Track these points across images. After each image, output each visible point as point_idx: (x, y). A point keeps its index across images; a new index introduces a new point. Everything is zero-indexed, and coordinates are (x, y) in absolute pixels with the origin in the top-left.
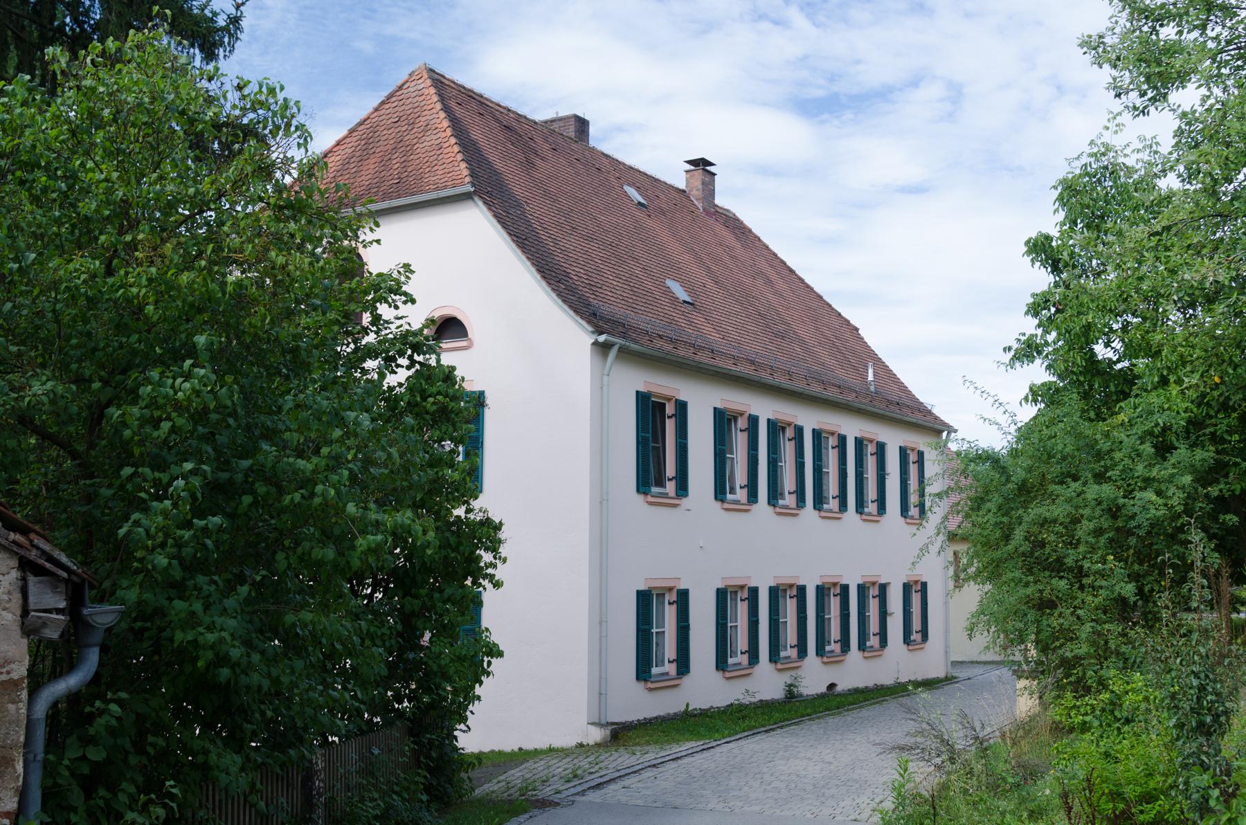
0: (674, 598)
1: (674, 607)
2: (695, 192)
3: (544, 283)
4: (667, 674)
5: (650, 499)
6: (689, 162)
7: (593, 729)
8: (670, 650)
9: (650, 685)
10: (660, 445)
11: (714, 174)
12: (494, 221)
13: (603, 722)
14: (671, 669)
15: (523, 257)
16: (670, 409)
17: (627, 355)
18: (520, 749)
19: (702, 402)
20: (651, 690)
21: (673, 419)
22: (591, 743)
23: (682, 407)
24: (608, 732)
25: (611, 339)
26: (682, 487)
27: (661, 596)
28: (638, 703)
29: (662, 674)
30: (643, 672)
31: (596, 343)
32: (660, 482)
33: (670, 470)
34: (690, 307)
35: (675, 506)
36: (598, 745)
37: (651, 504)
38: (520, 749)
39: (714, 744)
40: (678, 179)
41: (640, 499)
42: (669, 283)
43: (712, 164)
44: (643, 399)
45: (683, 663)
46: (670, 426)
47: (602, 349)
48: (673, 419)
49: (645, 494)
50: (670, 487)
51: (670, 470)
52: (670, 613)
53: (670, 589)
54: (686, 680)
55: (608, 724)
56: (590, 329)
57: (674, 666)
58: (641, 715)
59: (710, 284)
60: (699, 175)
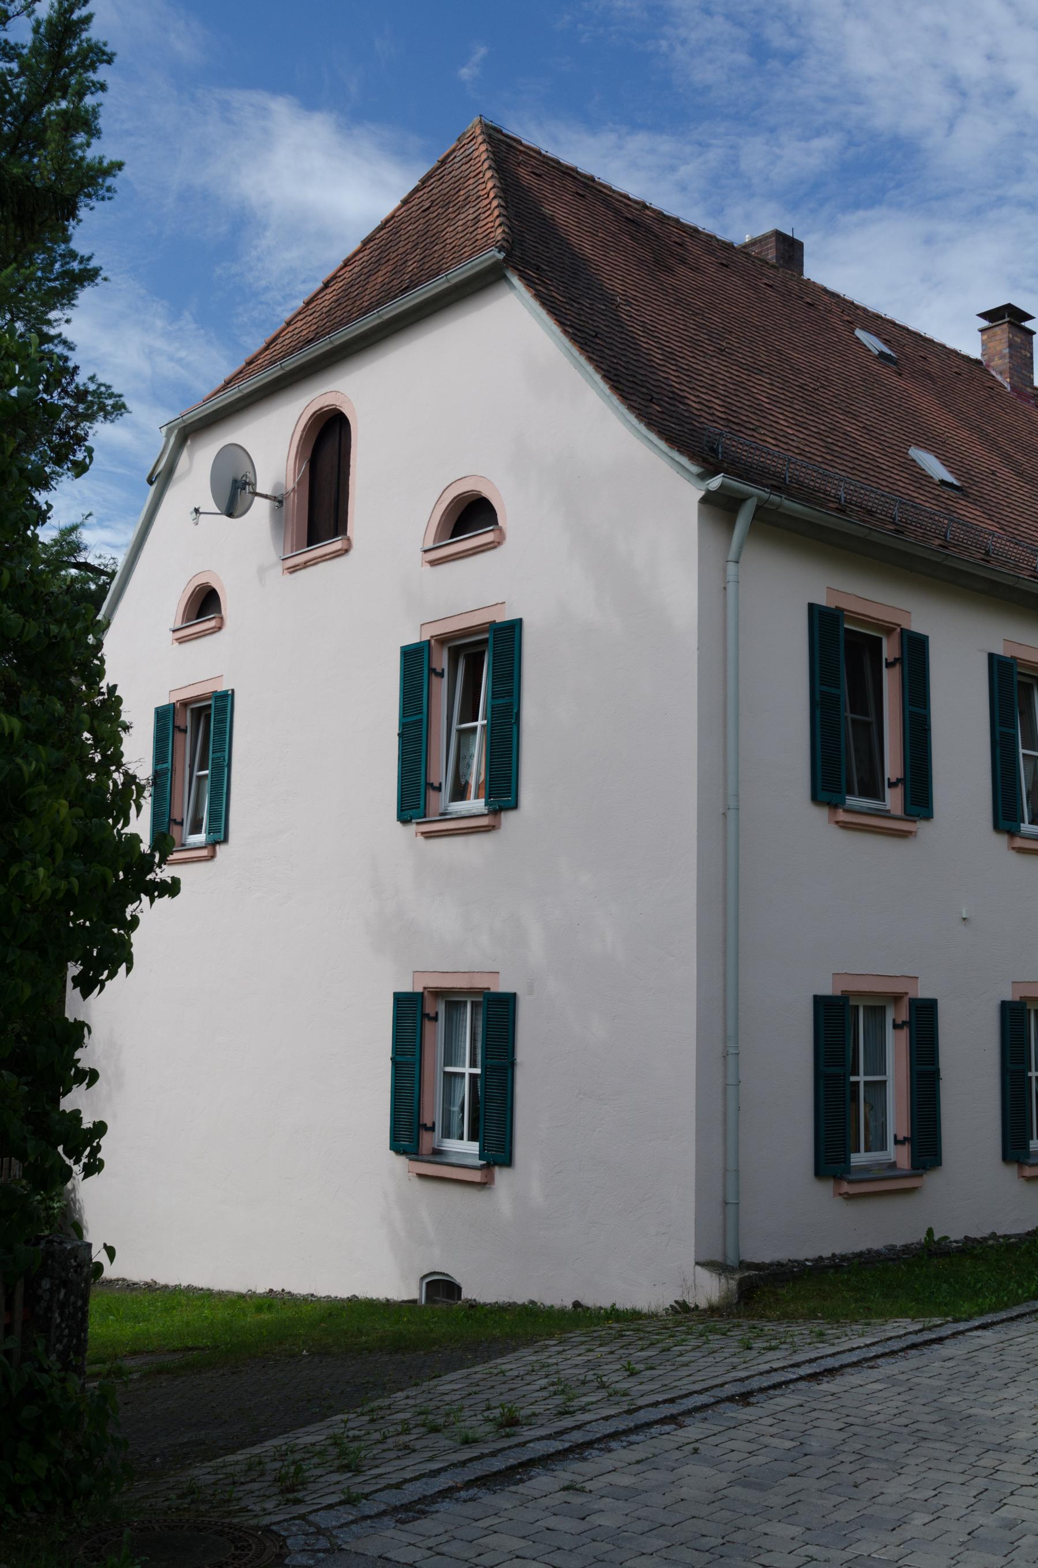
0: (904, 1015)
1: (904, 1033)
2: (997, 362)
3: (615, 400)
4: (893, 1165)
5: (842, 816)
6: (984, 315)
7: (703, 1274)
8: (897, 1118)
9: (846, 1188)
10: (872, 718)
11: (1033, 333)
12: (536, 305)
13: (732, 1261)
14: (899, 1155)
15: (582, 360)
16: (889, 650)
17: (777, 528)
18: (577, 1304)
19: (962, 651)
20: (849, 1197)
21: (897, 670)
22: (703, 1304)
23: (916, 650)
24: (733, 1284)
25: (735, 484)
26: (919, 800)
27: (876, 1013)
28: (808, 1221)
29: (880, 1165)
30: (831, 1156)
31: (708, 500)
32: (872, 789)
33: (892, 765)
34: (954, 493)
35: (904, 835)
36: (713, 1310)
37: (845, 826)
38: (577, 1304)
39: (962, 1326)
40: (968, 341)
41: (820, 815)
42: (915, 453)
43: (1029, 317)
44: (823, 622)
45: (926, 1145)
46: (891, 682)
47: (719, 508)
48: (897, 670)
49: (833, 805)
50: (893, 800)
51: (892, 765)
52: (896, 1047)
53: (897, 998)
54: (932, 1181)
55: (744, 1266)
56: (695, 469)
57: (905, 1150)
58: (806, 1251)
59: (1005, 473)
60: (1003, 332)
